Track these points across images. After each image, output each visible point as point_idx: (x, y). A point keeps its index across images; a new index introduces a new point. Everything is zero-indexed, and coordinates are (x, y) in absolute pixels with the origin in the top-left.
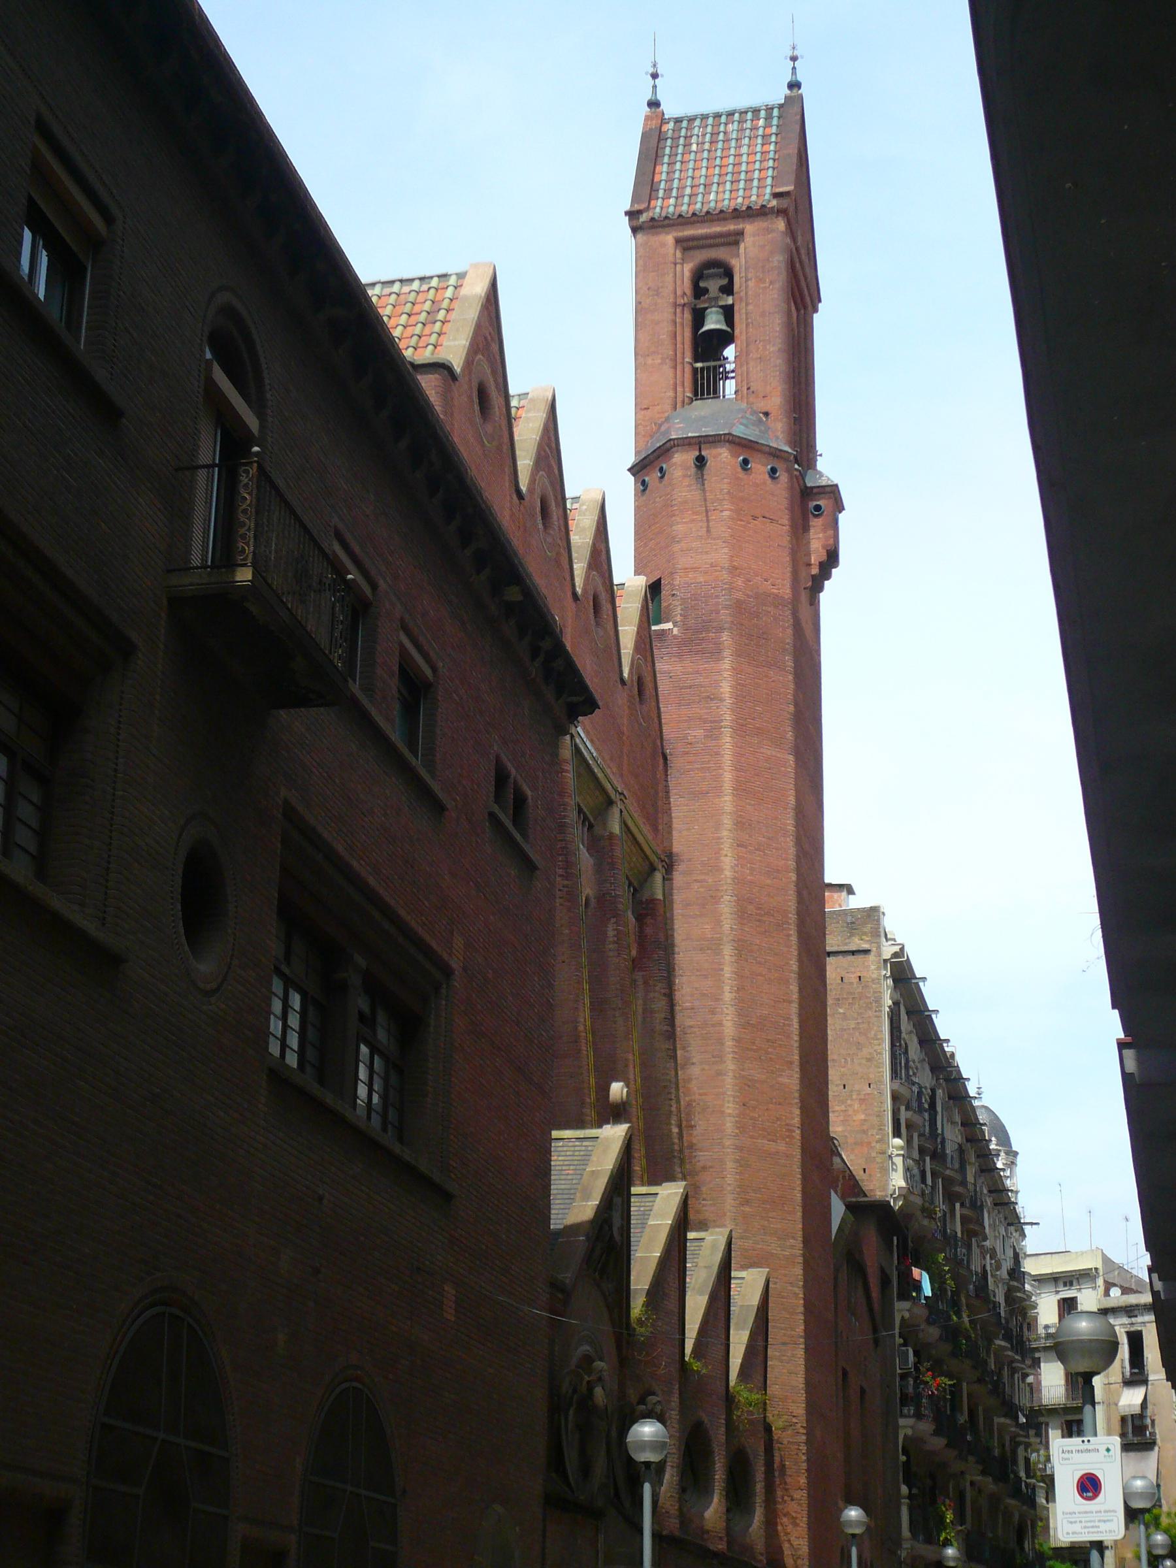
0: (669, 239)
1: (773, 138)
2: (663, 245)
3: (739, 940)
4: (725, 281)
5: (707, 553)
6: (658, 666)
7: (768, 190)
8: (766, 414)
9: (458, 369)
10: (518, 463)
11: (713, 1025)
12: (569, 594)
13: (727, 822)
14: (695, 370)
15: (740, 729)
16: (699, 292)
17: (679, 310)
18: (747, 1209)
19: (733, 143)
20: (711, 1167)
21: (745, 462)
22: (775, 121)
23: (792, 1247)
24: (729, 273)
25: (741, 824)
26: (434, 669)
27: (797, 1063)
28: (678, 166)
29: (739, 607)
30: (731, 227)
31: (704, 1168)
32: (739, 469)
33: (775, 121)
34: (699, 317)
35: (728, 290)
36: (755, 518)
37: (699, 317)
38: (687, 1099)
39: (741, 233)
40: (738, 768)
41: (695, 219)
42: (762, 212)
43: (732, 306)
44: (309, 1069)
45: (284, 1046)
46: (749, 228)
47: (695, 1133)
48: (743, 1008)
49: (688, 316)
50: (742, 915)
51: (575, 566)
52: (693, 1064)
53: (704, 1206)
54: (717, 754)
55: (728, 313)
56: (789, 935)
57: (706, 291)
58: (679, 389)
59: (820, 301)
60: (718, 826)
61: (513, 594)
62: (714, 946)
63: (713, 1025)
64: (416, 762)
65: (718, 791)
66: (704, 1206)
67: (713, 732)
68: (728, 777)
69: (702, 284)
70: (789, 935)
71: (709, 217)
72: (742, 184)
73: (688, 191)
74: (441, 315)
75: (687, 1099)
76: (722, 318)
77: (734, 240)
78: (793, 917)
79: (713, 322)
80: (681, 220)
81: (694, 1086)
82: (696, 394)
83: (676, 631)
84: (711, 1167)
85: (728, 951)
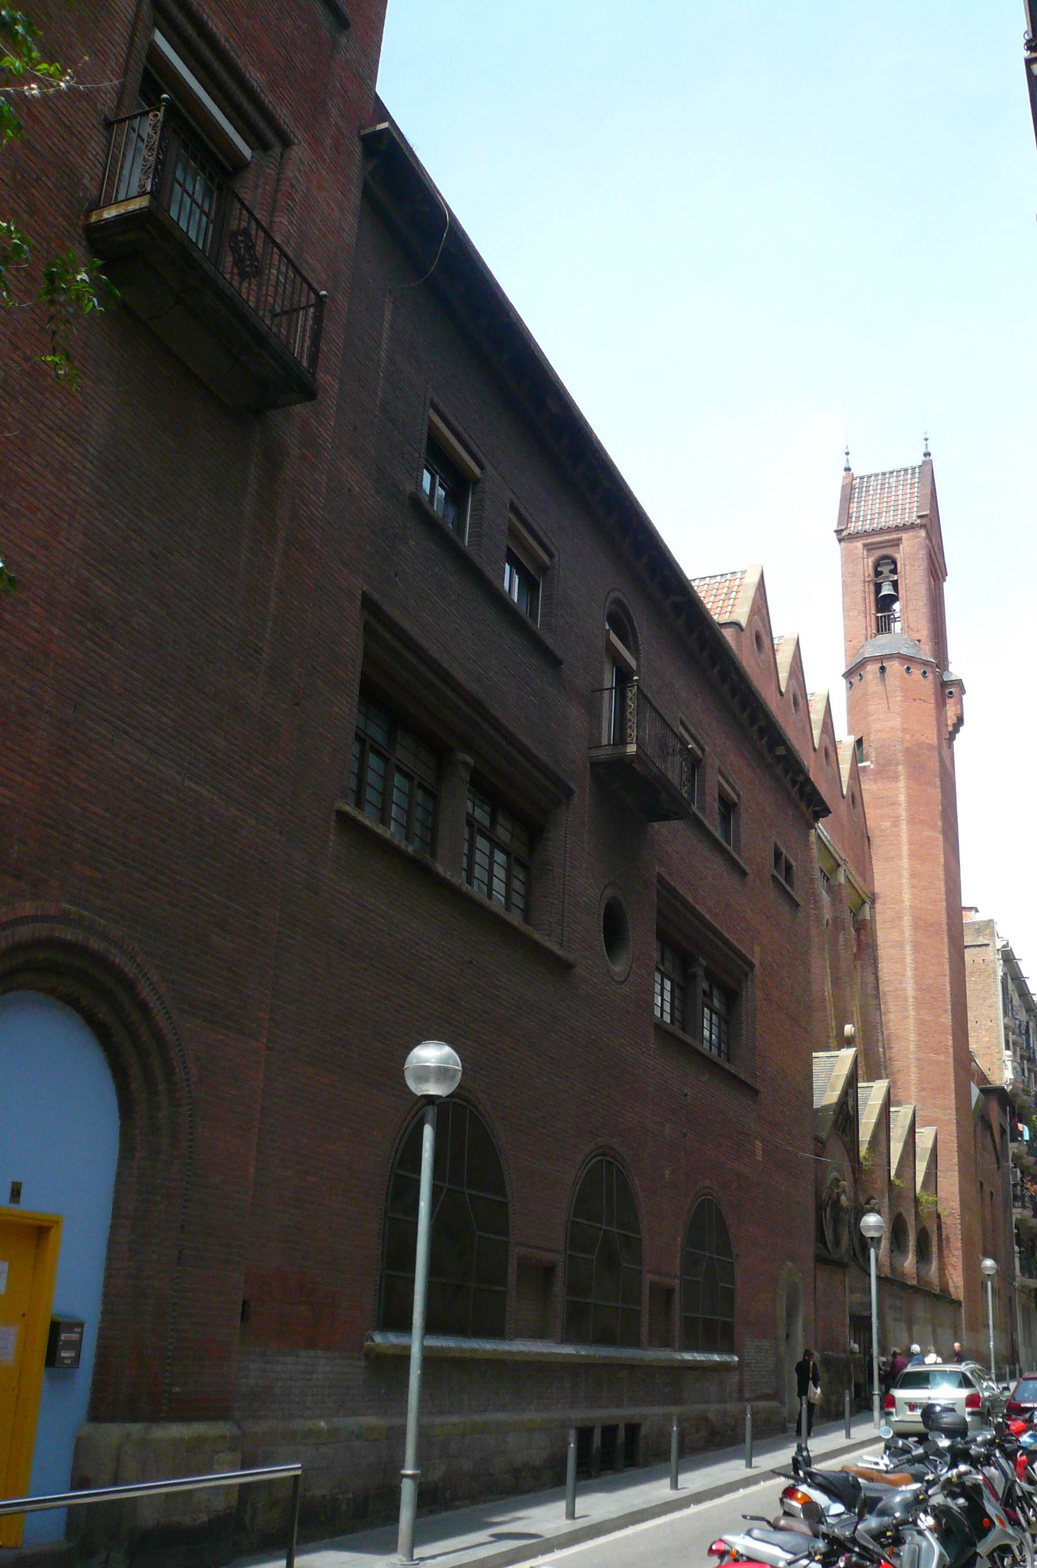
0: (859, 545)
1: (916, 485)
2: (856, 548)
3: (914, 941)
4: (892, 567)
5: (888, 721)
6: (863, 786)
7: (915, 514)
8: (919, 641)
9: (744, 624)
10: (780, 676)
11: (901, 990)
12: (811, 746)
13: (906, 874)
14: (877, 618)
15: (912, 821)
16: (878, 573)
17: (867, 584)
18: (923, 1093)
19: (894, 489)
20: (903, 1070)
21: (908, 669)
22: (917, 475)
23: (950, 1114)
24: (894, 562)
25: (913, 875)
26: (738, 796)
27: (950, 1010)
28: (863, 503)
29: (908, 751)
30: (894, 536)
31: (898, 1071)
32: (905, 673)
33: (917, 475)
34: (878, 588)
35: (894, 571)
36: (915, 700)
37: (878, 588)
38: (888, 1032)
39: (900, 539)
40: (911, 843)
41: (874, 532)
42: (912, 527)
43: (897, 580)
44: (676, 1023)
45: (662, 1010)
46: (905, 536)
47: (893, 1051)
48: (918, 980)
49: (872, 587)
50: (915, 927)
51: (814, 732)
52: (890, 1012)
53: (899, 1092)
54: (899, 835)
55: (895, 584)
56: (943, 938)
57: (881, 573)
58: (869, 629)
59: (947, 575)
60: (900, 876)
61: (781, 751)
62: (901, 946)
63: (901, 990)
64: (730, 849)
65: (899, 857)
66: (899, 1092)
67: (896, 824)
68: (905, 849)
69: (879, 569)
70: (943, 938)
71: (881, 531)
72: (900, 512)
73: (869, 517)
74: (733, 595)
75: (888, 1032)
76: (891, 587)
77: (897, 543)
78: (945, 927)
79: (887, 590)
80: (866, 534)
81: (891, 1025)
82: (878, 631)
83: (872, 766)
84: (903, 1070)
85: (908, 948)
